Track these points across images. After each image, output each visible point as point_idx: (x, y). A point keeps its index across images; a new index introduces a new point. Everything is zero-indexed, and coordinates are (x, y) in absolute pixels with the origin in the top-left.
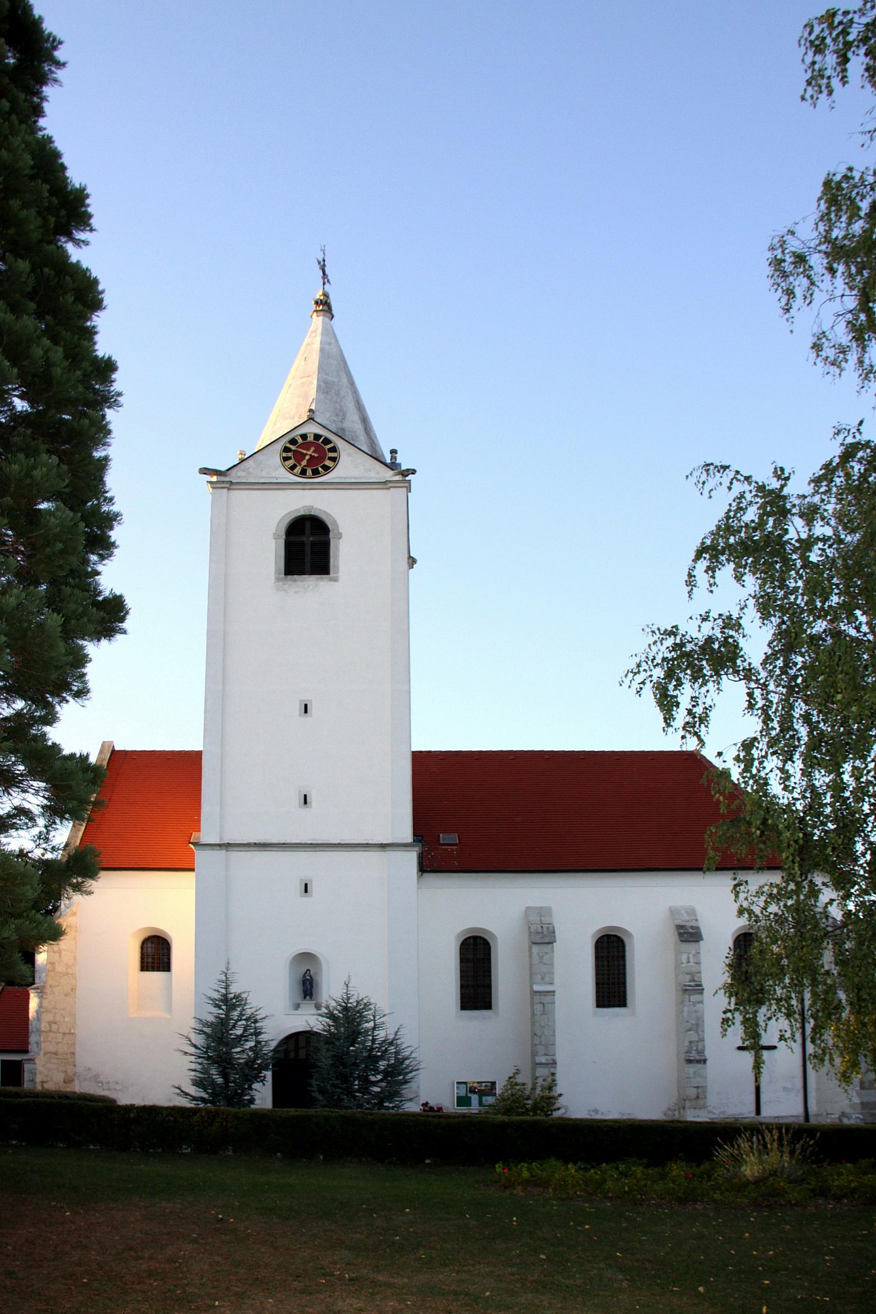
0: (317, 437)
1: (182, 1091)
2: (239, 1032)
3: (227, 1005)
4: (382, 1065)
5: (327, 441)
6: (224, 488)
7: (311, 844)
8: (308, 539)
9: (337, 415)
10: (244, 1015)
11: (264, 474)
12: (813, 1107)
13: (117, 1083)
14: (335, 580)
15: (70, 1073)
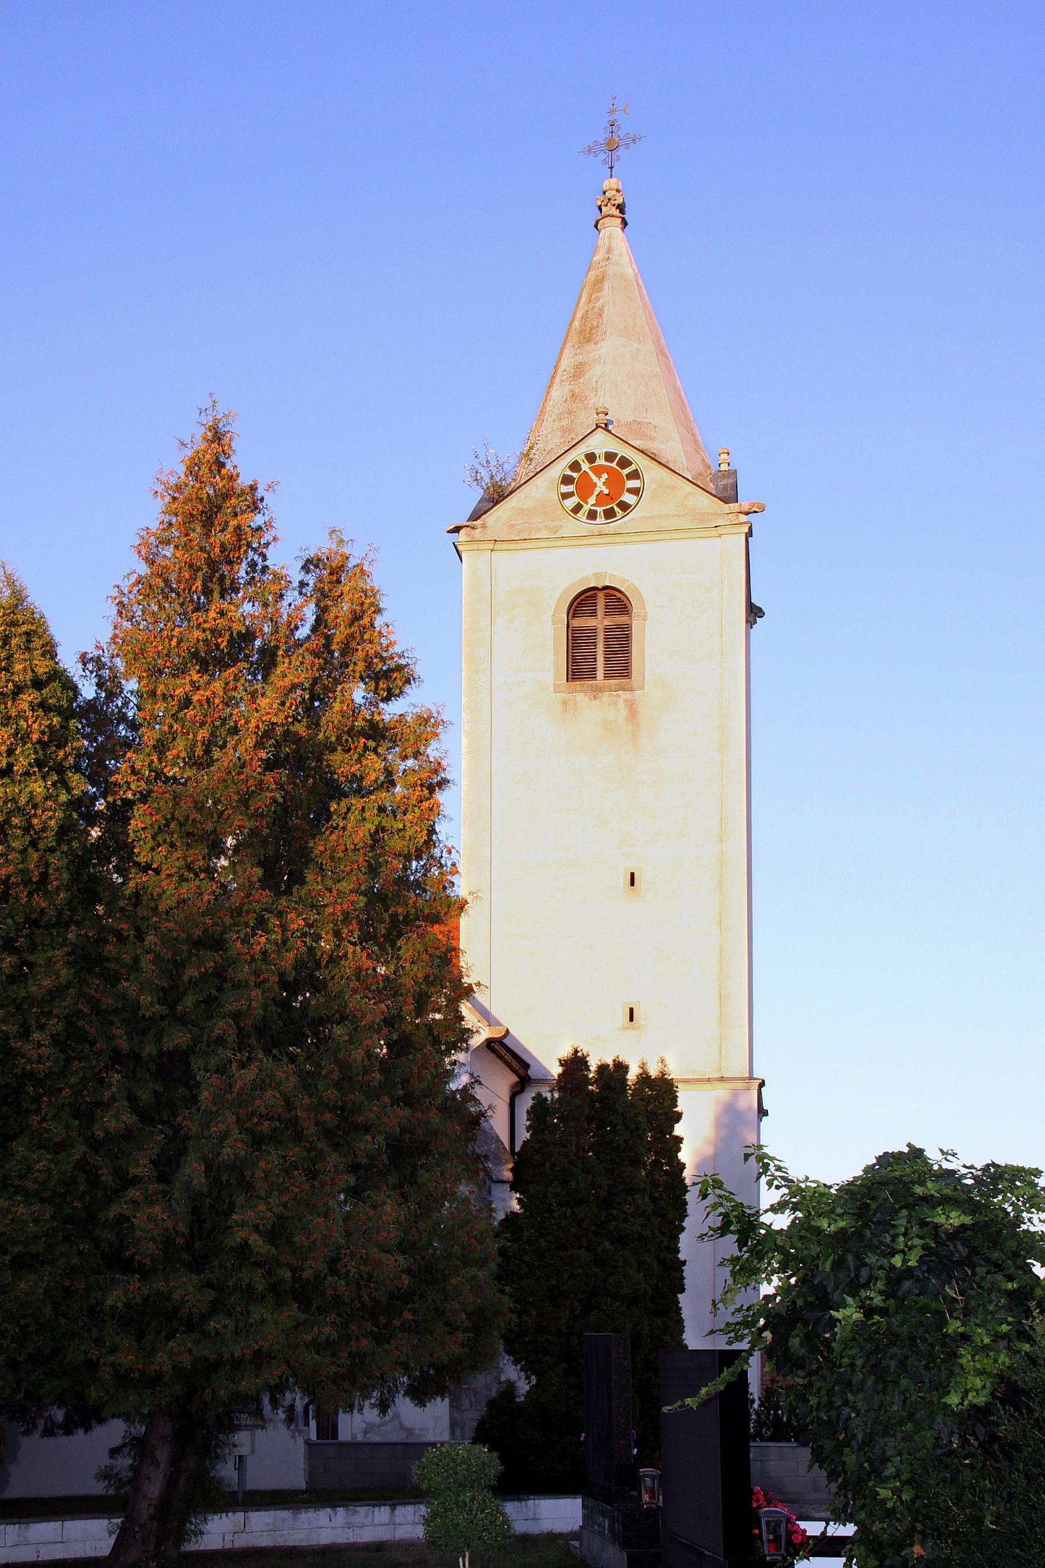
0: (610, 457)
5: (624, 463)
8: (600, 622)
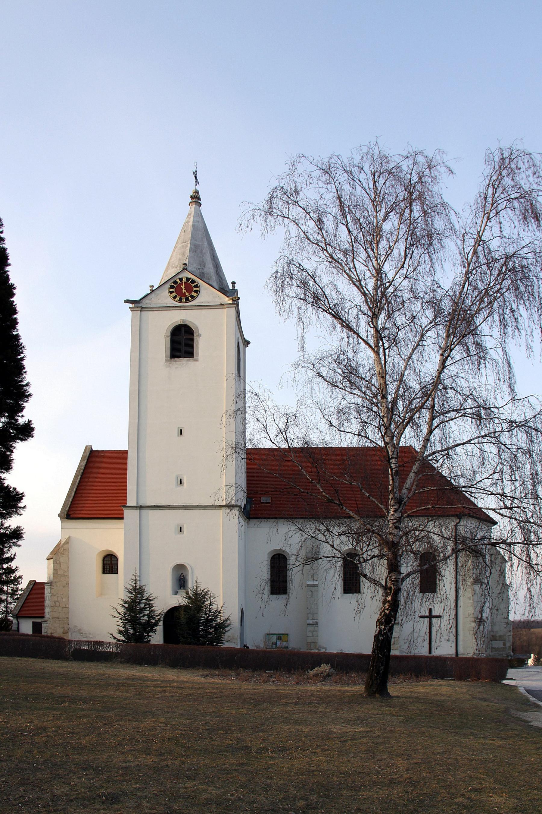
1: (113, 636)
2: (142, 606)
3: (136, 592)
4: (214, 624)
5: (193, 281)
6: (138, 310)
7: (183, 506)
9: (200, 265)
10: (144, 597)
11: (160, 301)
12: (461, 650)
13: (90, 634)
14: (197, 360)
15: (66, 629)
